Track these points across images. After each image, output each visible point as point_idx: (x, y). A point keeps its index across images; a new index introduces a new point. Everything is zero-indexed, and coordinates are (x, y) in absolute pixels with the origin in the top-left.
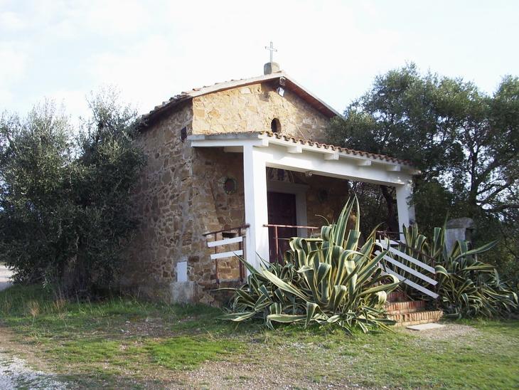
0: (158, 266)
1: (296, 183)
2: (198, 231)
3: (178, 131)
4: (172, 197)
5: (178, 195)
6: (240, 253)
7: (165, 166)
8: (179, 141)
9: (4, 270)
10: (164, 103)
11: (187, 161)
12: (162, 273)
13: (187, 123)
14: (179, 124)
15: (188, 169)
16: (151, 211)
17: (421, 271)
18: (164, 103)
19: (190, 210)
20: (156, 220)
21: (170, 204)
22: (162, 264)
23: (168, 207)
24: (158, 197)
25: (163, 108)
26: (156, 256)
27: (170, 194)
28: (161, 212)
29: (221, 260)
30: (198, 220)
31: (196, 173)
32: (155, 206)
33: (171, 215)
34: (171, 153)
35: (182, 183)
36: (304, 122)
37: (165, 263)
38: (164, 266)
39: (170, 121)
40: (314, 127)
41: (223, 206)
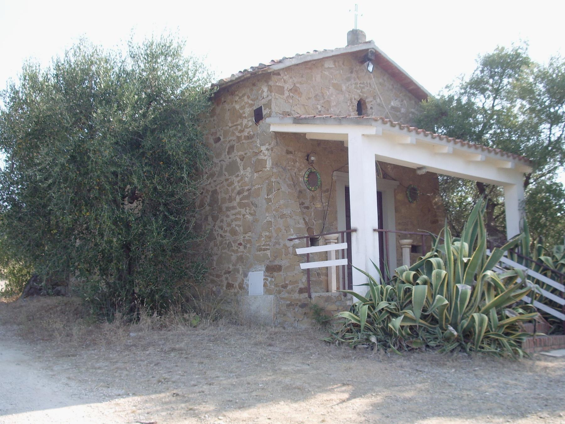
0: (218, 276)
1: (384, 178)
2: (280, 235)
3: (248, 111)
4: (239, 193)
5: (249, 190)
6: (345, 262)
7: (229, 153)
8: (250, 124)
9: (357, 239)
10: (32, 79)
11: (263, 148)
12: (225, 283)
13: (263, 102)
14: (250, 102)
15: (266, 158)
16: (208, 208)
17: (558, 293)
18: (233, 75)
19: (267, 210)
20: (215, 218)
21: (238, 199)
22: (225, 273)
23: (235, 204)
24: (219, 190)
25: (231, 81)
26: (215, 263)
27: (238, 189)
28: (224, 209)
29: (312, 269)
30: (281, 221)
31: (276, 164)
32: (214, 201)
33: (239, 213)
34: (239, 138)
35: (256, 175)
36: (392, 104)
37: (229, 272)
38: (228, 275)
39: (237, 98)
40: (403, 110)
41: (306, 205)
